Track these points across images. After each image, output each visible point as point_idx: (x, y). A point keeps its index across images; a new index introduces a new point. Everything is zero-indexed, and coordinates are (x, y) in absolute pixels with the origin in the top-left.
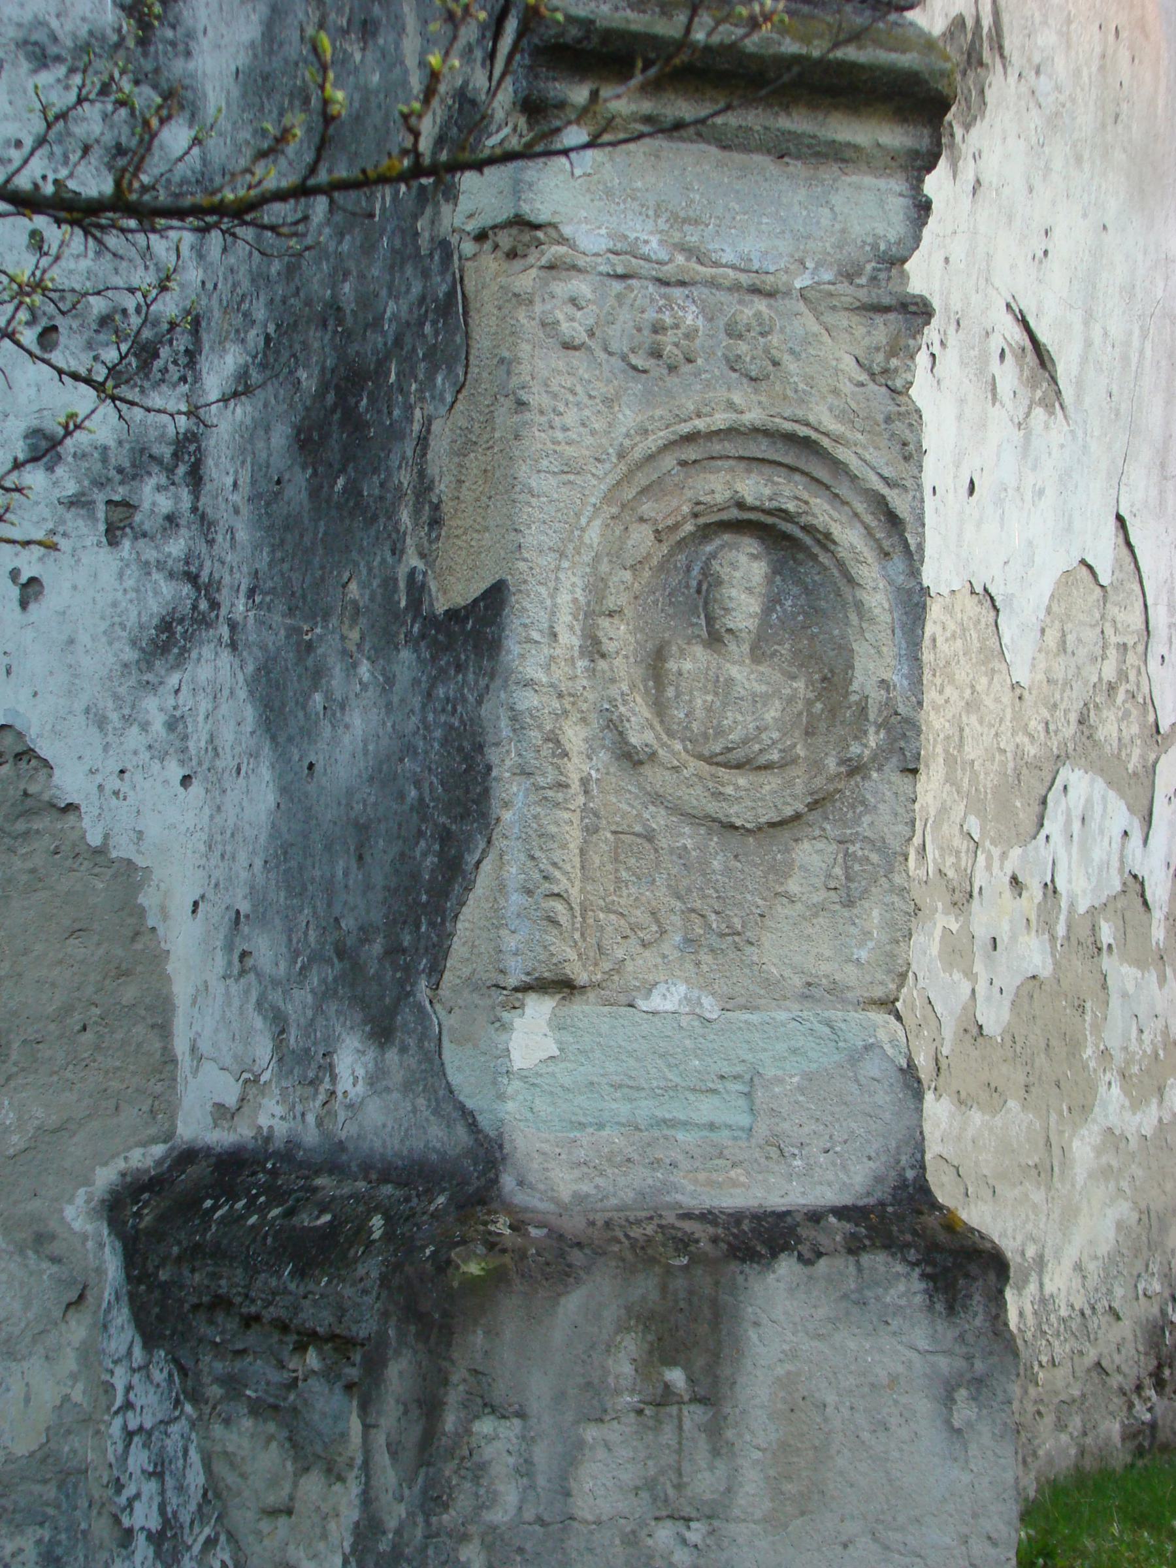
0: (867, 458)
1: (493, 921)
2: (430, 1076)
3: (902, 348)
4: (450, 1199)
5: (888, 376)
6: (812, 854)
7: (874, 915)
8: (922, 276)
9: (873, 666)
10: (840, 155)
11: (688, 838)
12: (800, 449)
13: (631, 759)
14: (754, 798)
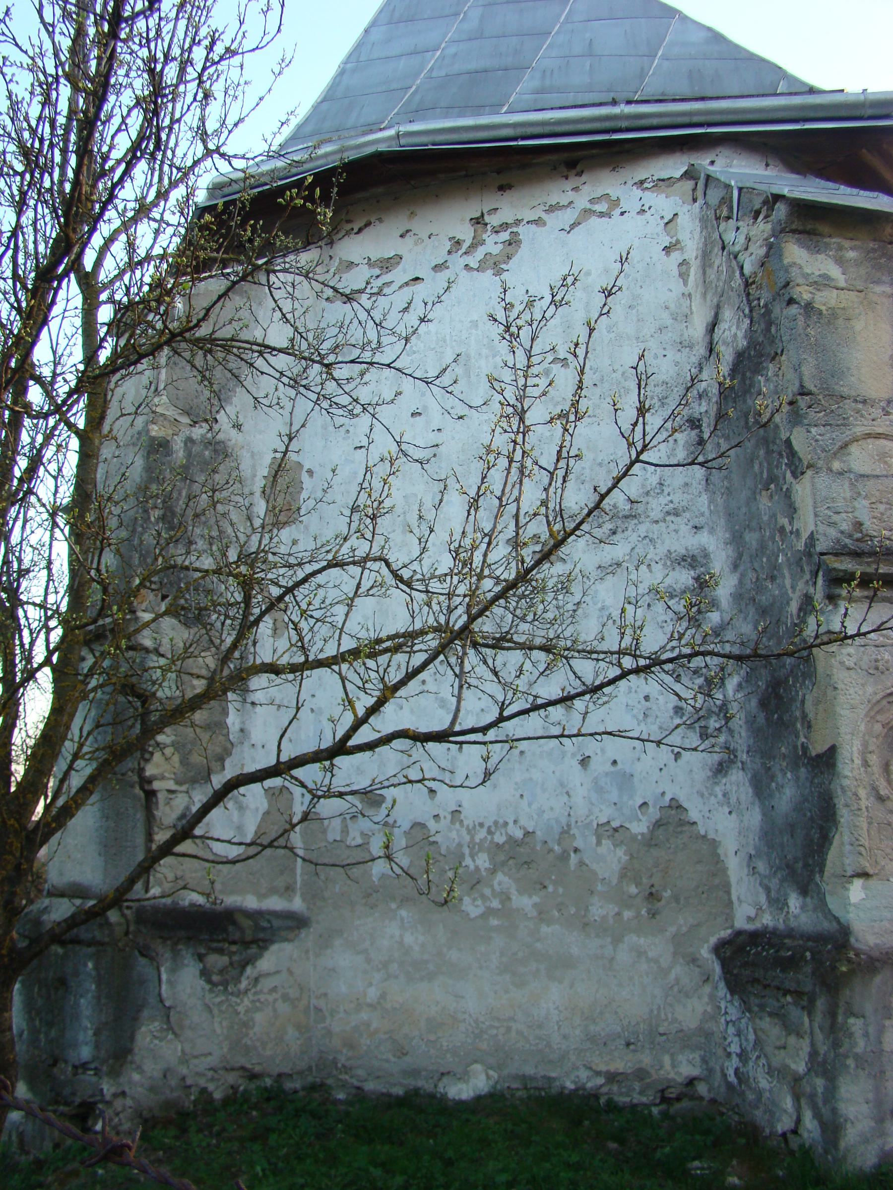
1: (841, 853)
2: (822, 906)
13: (881, 799)
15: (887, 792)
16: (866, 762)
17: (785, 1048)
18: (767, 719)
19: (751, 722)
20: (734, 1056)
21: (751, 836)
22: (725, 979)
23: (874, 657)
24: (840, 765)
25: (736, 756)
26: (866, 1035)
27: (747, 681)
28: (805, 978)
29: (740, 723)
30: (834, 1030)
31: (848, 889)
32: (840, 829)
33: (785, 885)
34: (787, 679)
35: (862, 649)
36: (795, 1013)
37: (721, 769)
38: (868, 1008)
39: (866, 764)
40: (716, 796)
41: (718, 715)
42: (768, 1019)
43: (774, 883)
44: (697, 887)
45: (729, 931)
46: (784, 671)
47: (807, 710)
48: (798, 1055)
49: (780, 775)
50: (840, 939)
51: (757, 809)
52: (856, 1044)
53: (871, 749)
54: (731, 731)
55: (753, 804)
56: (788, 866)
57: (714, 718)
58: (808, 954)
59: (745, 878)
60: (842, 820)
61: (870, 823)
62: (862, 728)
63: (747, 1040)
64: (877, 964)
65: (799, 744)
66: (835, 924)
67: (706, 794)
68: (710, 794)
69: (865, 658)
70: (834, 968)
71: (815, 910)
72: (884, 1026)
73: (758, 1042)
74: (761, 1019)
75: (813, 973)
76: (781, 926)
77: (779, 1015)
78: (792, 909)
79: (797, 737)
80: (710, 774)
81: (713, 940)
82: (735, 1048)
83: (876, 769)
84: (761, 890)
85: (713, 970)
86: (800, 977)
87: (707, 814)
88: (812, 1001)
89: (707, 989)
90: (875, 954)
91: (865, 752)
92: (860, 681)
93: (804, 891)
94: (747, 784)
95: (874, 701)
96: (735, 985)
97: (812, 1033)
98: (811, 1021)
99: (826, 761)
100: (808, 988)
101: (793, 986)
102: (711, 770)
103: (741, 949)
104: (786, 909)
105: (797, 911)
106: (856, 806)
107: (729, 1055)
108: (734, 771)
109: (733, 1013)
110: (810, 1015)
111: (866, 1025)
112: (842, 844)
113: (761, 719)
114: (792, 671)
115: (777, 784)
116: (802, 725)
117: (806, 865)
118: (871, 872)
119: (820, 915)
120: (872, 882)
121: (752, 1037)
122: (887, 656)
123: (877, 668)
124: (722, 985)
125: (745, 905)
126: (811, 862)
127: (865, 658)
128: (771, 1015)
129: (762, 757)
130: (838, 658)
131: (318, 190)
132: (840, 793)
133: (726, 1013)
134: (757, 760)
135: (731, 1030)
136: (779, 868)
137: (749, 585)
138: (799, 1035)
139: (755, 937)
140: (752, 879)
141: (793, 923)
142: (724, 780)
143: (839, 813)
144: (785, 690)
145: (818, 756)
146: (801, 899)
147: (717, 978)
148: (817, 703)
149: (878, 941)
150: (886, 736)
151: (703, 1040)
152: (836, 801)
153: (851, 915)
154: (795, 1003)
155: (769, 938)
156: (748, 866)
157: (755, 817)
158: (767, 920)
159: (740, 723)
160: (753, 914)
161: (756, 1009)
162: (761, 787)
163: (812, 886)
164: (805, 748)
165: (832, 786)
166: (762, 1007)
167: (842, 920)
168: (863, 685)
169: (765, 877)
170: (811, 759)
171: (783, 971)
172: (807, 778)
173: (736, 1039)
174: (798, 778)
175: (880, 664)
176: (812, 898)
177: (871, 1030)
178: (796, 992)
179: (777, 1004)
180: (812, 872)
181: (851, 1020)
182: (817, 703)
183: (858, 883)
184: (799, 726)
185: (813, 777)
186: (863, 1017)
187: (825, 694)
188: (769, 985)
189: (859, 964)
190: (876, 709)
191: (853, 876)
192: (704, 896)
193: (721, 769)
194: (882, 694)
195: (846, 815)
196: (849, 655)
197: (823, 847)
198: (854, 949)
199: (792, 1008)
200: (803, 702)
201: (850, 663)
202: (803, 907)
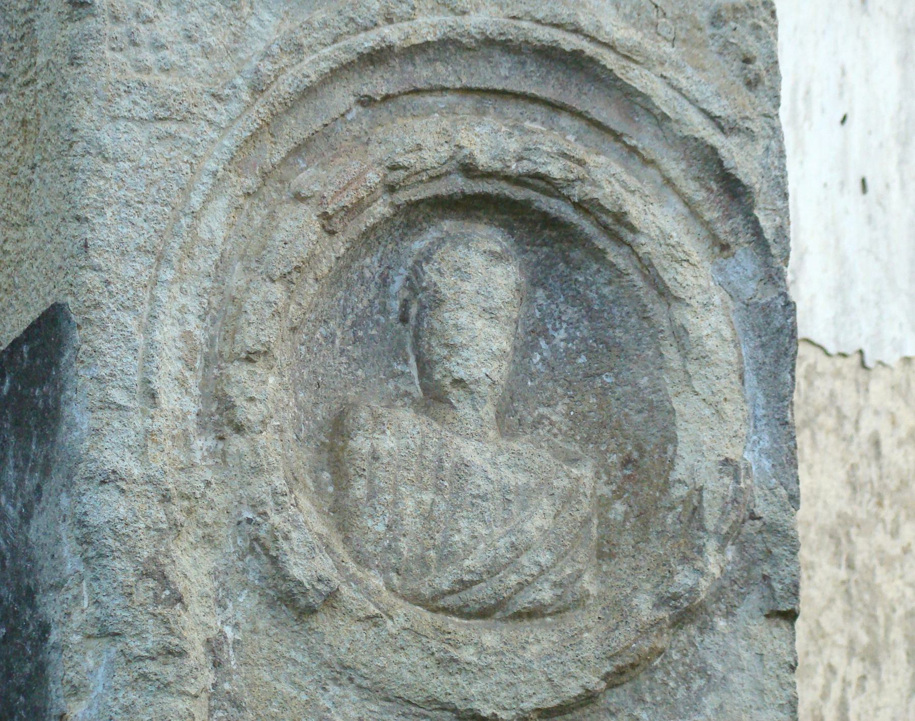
0: (683, 84)
9: (710, 435)
13: (295, 604)
15: (324, 565)
16: (226, 405)
24: (79, 416)
39: (222, 417)
53: (249, 339)
62: (215, 223)
83: (277, 446)
91: (220, 355)
95: (285, 86)
106: (153, 639)
131: (5, 389)
132: (72, 564)
143: (62, 670)
150: (338, 278)
152: (51, 607)
190: (296, 129)
195: (98, 683)
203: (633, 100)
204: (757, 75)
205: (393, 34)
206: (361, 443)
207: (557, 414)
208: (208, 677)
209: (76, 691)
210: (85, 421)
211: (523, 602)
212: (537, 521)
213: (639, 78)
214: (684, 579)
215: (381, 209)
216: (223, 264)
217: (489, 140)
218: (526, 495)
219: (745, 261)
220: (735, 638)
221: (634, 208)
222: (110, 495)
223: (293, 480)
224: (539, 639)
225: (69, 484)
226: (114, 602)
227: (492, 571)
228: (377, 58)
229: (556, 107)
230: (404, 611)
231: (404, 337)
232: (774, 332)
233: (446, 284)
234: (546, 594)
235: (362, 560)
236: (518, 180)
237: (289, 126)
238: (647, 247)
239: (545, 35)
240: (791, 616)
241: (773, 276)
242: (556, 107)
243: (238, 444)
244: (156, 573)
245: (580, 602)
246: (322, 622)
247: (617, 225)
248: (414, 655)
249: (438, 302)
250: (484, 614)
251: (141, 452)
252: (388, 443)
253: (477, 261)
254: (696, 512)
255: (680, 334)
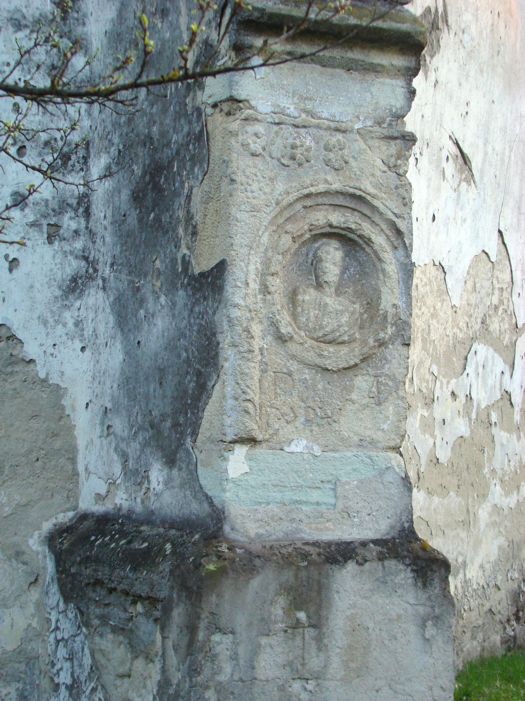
0: (387, 205)
1: (220, 412)
2: (192, 481)
3: (403, 156)
4: (201, 536)
5: (396, 168)
6: (362, 382)
7: (390, 409)
8: (411, 123)
9: (390, 298)
10: (375, 69)
11: (307, 374)
12: (357, 201)
13: (282, 339)
14: (337, 357)
15: (290, 329)
16: (266, 287)
17: (129, 676)
18: (140, 220)
19: (119, 221)
20: (63, 688)
21: (108, 383)
22: (59, 580)
23: (290, 141)
24: (229, 289)
25: (96, 270)
26: (234, 657)
27: (118, 164)
28: (159, 579)
29: (105, 222)
30: (193, 650)
31: (226, 459)
32: (223, 377)
33: (148, 450)
34: (170, 163)
35: (276, 128)
36: (145, 627)
37: (75, 287)
38: (240, 621)
39: (265, 290)
40: (65, 325)
41: (76, 210)
42: (110, 636)
43: (133, 449)
44: (30, 451)
45: (71, 514)
46: (168, 152)
47: (193, 210)
48: (145, 687)
49: (151, 299)
50: (208, 528)
51: (118, 345)
52: (220, 670)
53: (273, 269)
54: (91, 234)
55: (113, 337)
56: (152, 426)
57: (71, 213)
58: (168, 546)
59: (97, 442)
60: (226, 365)
61: (264, 371)
62: (265, 239)
63: (81, 666)
64: (258, 562)
65: (179, 256)
66: (206, 505)
67: (51, 320)
68: (57, 322)
69: (279, 141)
70: (198, 566)
71: (182, 486)
72: (259, 646)
73: (95, 668)
74: (101, 636)
75: (171, 572)
76: (139, 508)
77: (125, 631)
78: (154, 484)
79: (177, 246)
80: (58, 293)
81: (47, 526)
82: (65, 678)
83: (279, 298)
84: (115, 457)
85: (45, 568)
86: (155, 577)
87: (51, 350)
88: (167, 611)
89: (35, 594)
90: (256, 548)
91: (265, 274)
92: (268, 174)
93: (171, 462)
94: (108, 310)
95: (284, 203)
96: (71, 588)
97: (163, 655)
98: (164, 638)
99: (211, 282)
100: (163, 594)
101: (143, 590)
102: (60, 287)
103: (84, 539)
104: (146, 485)
105: (161, 491)
107: (57, 686)
108: (92, 291)
109: (67, 628)
110: (162, 629)
111: (236, 644)
112: (224, 397)
113: (133, 219)
114: (178, 153)
115: (147, 311)
116: (186, 229)
117: (176, 425)
118: (260, 437)
119: (188, 492)
120: (260, 451)
121: (87, 661)
122: (309, 142)
123: (293, 158)
124: (54, 588)
125: (93, 477)
126: (182, 420)
127: (279, 141)
128: (115, 630)
129: (130, 273)
130: (240, 138)
132: (226, 327)
133: (57, 628)
134: (123, 276)
135: (62, 652)
136: (141, 428)
137: (131, 22)
138: (149, 659)
139: (103, 523)
140: (105, 442)
141: (154, 505)
142: (78, 304)
144: (166, 179)
145: (202, 275)
146: (166, 471)
147: (48, 579)
148: (207, 200)
149: (261, 531)
151: (23, 667)
153: (228, 494)
154: (147, 614)
155: (122, 524)
156: (102, 423)
157: (114, 357)
158: (121, 499)
159: (105, 222)
160: (103, 492)
161: (96, 622)
162: (126, 314)
163: (181, 454)
164: (186, 263)
165: (216, 318)
166: (104, 619)
167: (216, 501)
168: (271, 180)
169: (123, 439)
170: (192, 278)
171: (134, 569)
172: (186, 305)
173: (67, 665)
174: (174, 304)
175: (298, 152)
176: (180, 469)
177: (242, 650)
178: (149, 598)
179: (123, 615)
180: (183, 435)
181: (216, 637)
182: (207, 200)
183: (241, 451)
184: (181, 231)
185: (194, 305)
186: (233, 632)
187: (218, 188)
188: (115, 589)
189: (233, 561)
190: (286, 214)
191: (235, 442)
192: (40, 463)
193: (75, 287)
194: (295, 195)
195: (232, 358)
196: (256, 135)
197: (199, 400)
198: (227, 540)
199: (141, 619)
200: (189, 198)
201: (256, 146)
202: (167, 483)
203: (374, 208)
204: (407, 203)
205: (313, 190)
206: (300, 297)
207: (350, 290)
208: (260, 357)
209: (226, 360)
210: (230, 290)
211: (340, 340)
212: (344, 319)
213: (376, 203)
214: (382, 335)
215: (307, 236)
216: (266, 250)
217: (336, 218)
218: (342, 312)
219: (401, 252)
220: (394, 351)
221: (373, 237)
222: (236, 310)
223: (282, 307)
224: (344, 350)
225: (225, 307)
226: (236, 338)
227: (333, 331)
228: (308, 196)
229: (354, 210)
230: (310, 342)
231: (312, 269)
232: (408, 270)
233: (323, 256)
234: (346, 338)
235: (299, 328)
236: (343, 229)
237: (286, 214)
238: (376, 247)
239: (352, 191)
240: (408, 345)
241: (408, 256)
242: (354, 210)
243: (269, 297)
244: (247, 330)
245: (355, 340)
246: (289, 344)
247: (369, 241)
248: (312, 353)
249: (321, 260)
250: (330, 343)
251: (244, 299)
252: (307, 298)
253: (332, 250)
254: (385, 317)
255: (383, 271)
